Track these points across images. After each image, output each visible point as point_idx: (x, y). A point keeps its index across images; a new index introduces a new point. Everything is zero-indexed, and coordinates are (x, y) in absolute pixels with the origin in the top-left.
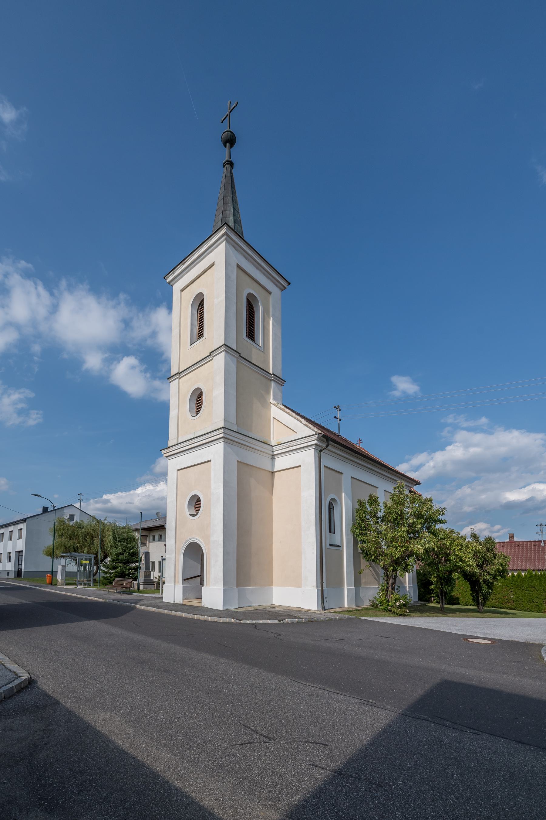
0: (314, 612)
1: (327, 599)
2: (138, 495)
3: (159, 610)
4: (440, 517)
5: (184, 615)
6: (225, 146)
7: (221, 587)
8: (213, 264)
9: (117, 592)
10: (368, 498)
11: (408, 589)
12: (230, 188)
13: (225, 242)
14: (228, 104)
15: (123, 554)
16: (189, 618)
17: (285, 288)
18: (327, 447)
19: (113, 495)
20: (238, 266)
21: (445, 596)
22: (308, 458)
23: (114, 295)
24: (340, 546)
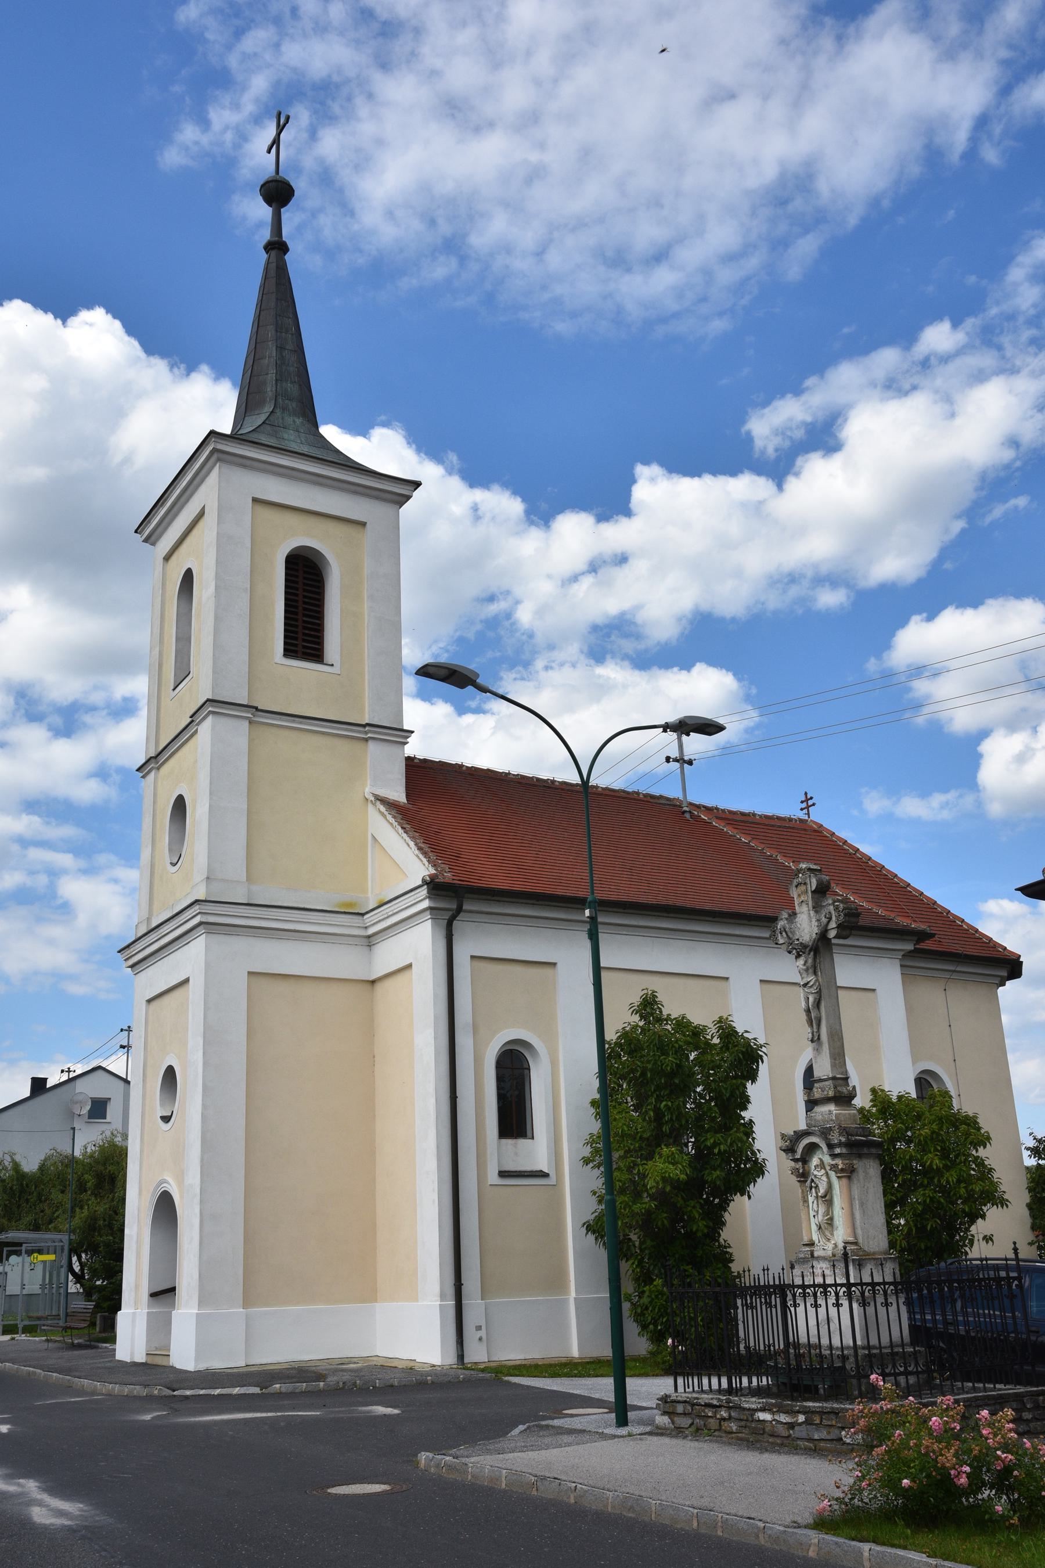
1: (483, 1333)
24: (544, 1175)
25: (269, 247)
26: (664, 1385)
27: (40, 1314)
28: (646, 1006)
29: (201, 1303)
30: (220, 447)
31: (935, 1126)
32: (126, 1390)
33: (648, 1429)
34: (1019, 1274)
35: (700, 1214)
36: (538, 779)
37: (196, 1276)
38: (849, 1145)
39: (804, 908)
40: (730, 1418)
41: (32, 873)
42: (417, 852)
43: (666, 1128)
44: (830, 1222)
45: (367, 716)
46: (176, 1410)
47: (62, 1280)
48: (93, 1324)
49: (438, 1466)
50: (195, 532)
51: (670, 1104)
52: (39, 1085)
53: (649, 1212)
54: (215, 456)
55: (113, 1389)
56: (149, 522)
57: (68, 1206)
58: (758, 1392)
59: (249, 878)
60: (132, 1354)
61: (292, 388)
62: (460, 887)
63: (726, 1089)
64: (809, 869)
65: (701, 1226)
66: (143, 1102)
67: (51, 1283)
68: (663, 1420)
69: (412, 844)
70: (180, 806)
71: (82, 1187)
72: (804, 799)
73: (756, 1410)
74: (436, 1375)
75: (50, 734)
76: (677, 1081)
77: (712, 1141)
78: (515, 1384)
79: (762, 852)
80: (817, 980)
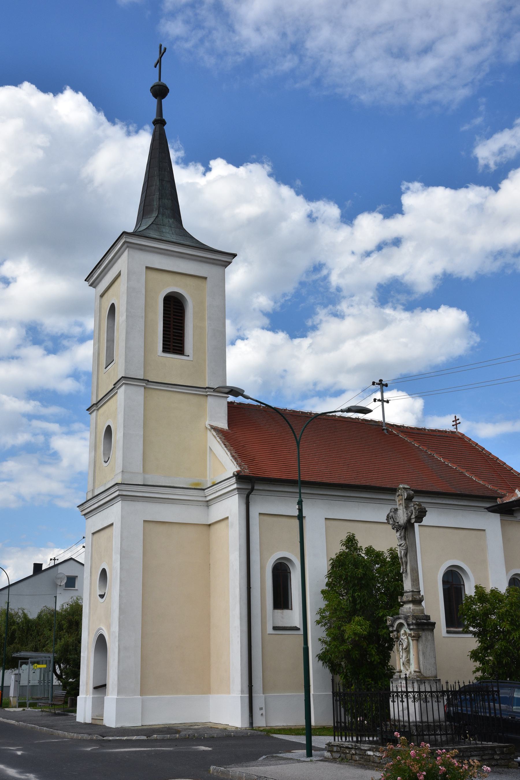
1: (263, 711)
25: (155, 122)
26: (330, 739)
27: (39, 696)
28: (349, 542)
29: (119, 693)
30: (128, 240)
31: (508, 607)
32: (80, 736)
33: (321, 758)
34: (498, 689)
35: (375, 652)
36: (302, 413)
37: (116, 679)
38: (417, 624)
39: (401, 507)
40: (356, 754)
41: (35, 435)
42: (231, 458)
43: (358, 607)
44: (408, 661)
45: (207, 383)
46: (103, 746)
47: (50, 678)
48: (66, 703)
49: (217, 772)
50: (116, 284)
51: (359, 594)
52: (38, 568)
53: (348, 651)
55: (74, 736)
56: (92, 276)
57: (53, 638)
58: (370, 742)
59: (144, 471)
60: (85, 719)
61: (168, 202)
62: (253, 477)
63: (392, 586)
64: (404, 488)
65: (376, 658)
66: (88, 589)
67: (44, 680)
68: (327, 754)
69: (229, 453)
70: (109, 430)
71: (61, 628)
72: (454, 420)
73: (367, 750)
74: (236, 732)
75: (45, 353)
76: (363, 582)
77: (382, 614)
78: (275, 738)
79: (426, 452)
80: (406, 543)
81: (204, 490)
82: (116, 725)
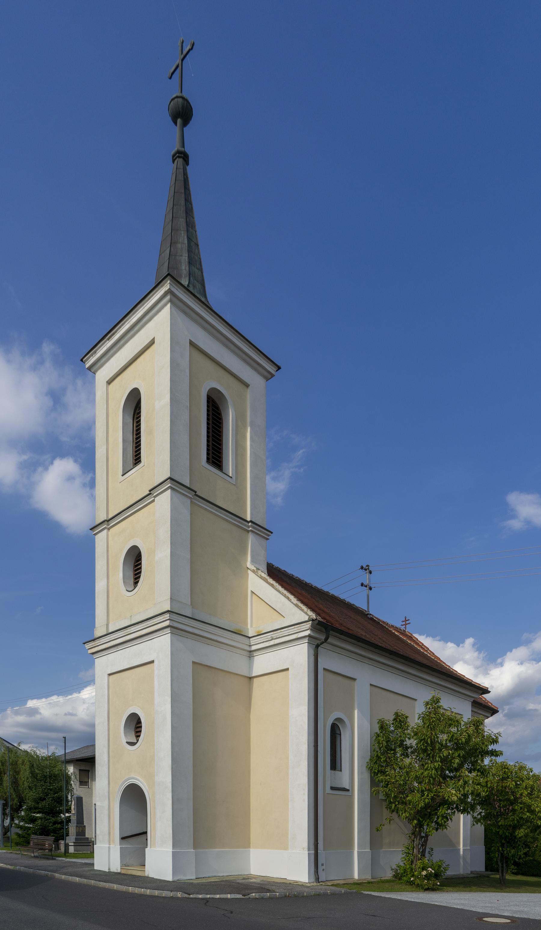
0: (303, 885)
1: (324, 867)
2: (84, 701)
3: (85, 881)
4: (491, 747)
5: (115, 887)
6: (176, 123)
7: (169, 849)
8: (152, 342)
9: (34, 857)
10: (393, 717)
11: (461, 853)
12: (183, 202)
13: (169, 305)
14: (179, 44)
15: (44, 799)
16: (122, 892)
17: (272, 376)
18: (326, 640)
19: (44, 700)
20: (192, 343)
21: (507, 862)
22: (298, 656)
23: (33, 347)
24: (348, 790)
54: (168, 297)
55: (114, 887)
56: (95, 352)
81: (250, 638)
82: (173, 878)
